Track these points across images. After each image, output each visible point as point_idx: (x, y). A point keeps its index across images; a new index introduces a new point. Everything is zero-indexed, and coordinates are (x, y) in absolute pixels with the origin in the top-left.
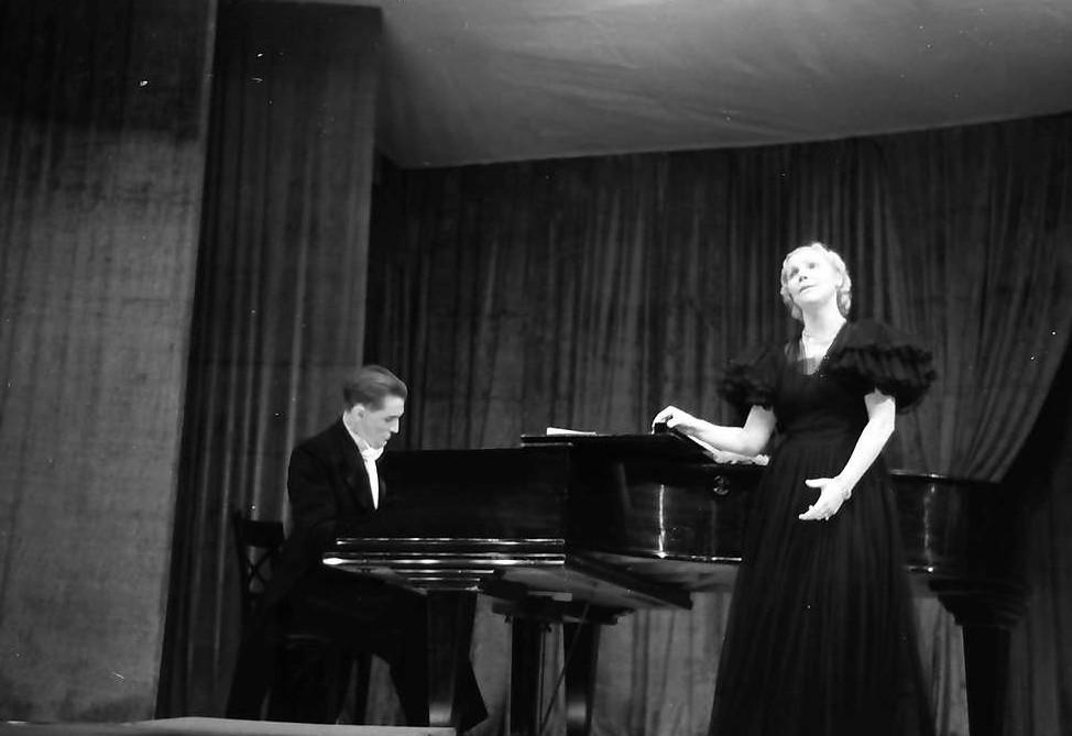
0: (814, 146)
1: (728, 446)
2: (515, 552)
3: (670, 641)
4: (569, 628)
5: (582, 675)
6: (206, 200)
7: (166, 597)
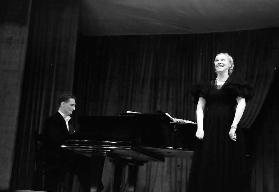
0: (201, 34)
2: (116, 145)
3: (157, 170)
4: (130, 167)
5: (133, 180)
6: (28, 43)
7: (13, 156)
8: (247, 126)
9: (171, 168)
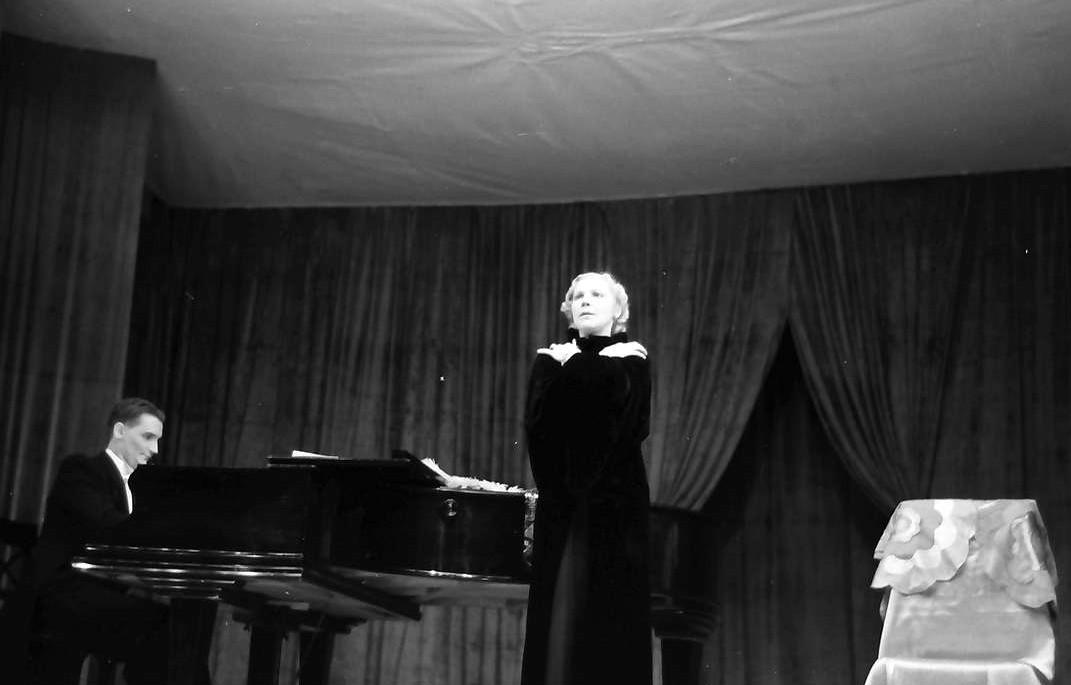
2: (257, 564)
3: (401, 650)
4: (305, 639)
8: (692, 505)
9: (446, 641)
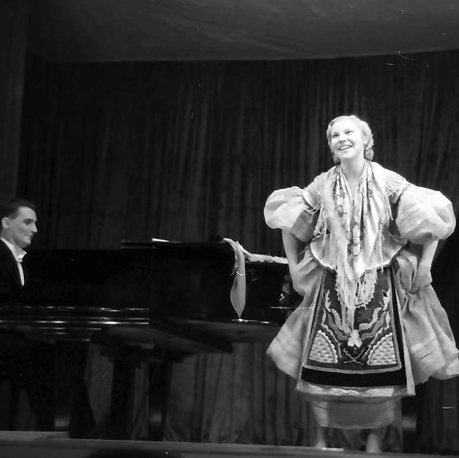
1: (395, 284)
